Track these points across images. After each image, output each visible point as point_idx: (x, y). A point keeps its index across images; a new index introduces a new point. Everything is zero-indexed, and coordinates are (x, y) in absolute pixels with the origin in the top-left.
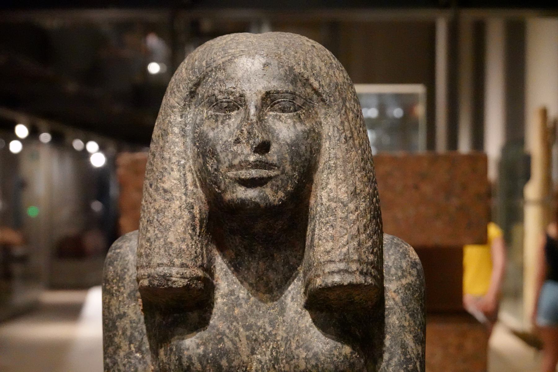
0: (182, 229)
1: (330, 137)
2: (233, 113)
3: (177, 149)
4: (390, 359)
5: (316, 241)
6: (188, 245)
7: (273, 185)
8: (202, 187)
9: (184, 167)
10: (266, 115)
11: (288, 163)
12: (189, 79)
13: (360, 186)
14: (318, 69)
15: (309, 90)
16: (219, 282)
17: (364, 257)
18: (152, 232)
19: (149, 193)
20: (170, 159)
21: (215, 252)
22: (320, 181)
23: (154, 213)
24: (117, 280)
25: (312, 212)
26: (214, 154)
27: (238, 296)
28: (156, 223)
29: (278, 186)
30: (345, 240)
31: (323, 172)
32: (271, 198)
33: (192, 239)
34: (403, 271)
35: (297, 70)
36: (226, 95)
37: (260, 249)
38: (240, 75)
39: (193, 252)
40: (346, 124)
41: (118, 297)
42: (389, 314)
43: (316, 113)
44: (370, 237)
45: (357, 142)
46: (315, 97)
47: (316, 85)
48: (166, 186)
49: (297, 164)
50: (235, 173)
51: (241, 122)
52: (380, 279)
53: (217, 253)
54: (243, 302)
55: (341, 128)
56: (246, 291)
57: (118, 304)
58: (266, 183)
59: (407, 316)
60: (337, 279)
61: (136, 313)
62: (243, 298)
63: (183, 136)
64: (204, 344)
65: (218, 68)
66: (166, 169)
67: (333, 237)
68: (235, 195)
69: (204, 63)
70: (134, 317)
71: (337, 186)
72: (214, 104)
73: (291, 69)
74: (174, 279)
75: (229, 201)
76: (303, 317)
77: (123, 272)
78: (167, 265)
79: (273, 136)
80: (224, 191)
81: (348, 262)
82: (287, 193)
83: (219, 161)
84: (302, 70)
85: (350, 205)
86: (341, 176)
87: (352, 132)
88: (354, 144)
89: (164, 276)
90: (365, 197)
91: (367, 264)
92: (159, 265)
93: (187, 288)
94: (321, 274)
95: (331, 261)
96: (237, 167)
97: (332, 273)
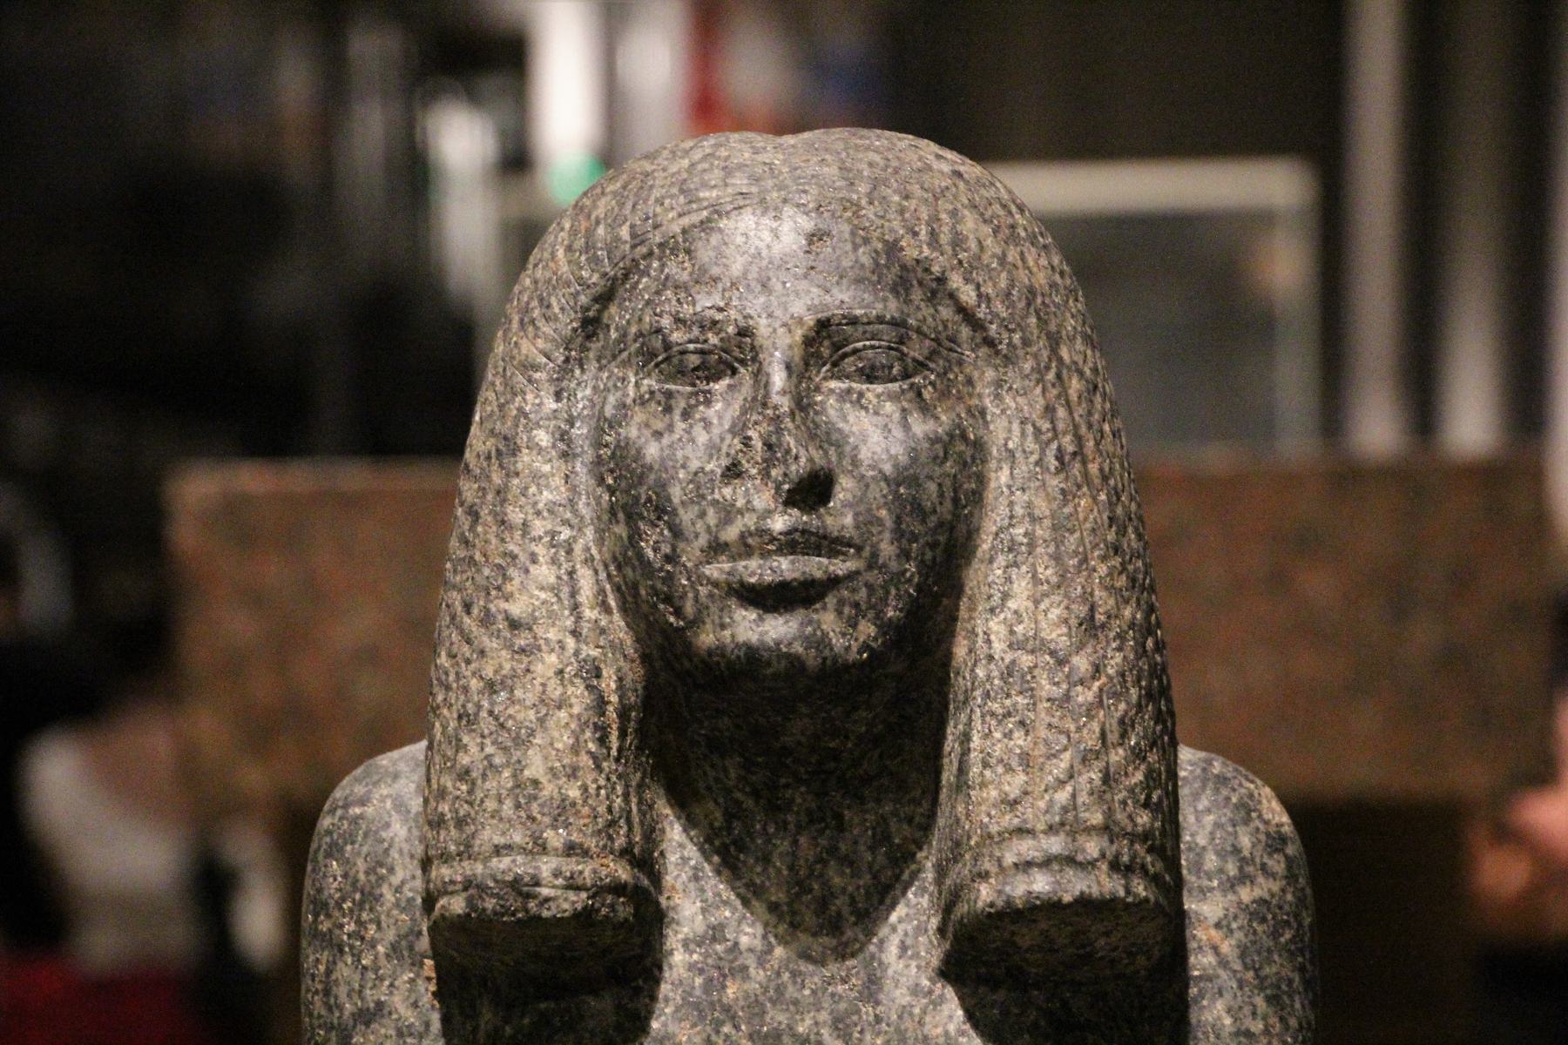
0: (566, 740)
1: (1011, 453)
2: (719, 386)
5: (975, 770)
6: (585, 788)
7: (841, 603)
8: (624, 610)
9: (569, 552)
10: (818, 389)
11: (887, 535)
12: (581, 281)
13: (1105, 602)
14: (973, 245)
15: (946, 312)
16: (677, 899)
17: (1120, 816)
18: (474, 749)
19: (462, 632)
21: (664, 809)
22: (985, 589)
23: (480, 692)
24: (354, 902)
25: (960, 684)
26: (662, 510)
27: (736, 944)
28: (487, 723)
29: (856, 605)
30: (1064, 765)
31: (991, 561)
32: (838, 642)
33: (599, 768)
34: (1243, 861)
35: (911, 252)
36: (696, 331)
37: (801, 798)
38: (736, 268)
39: (602, 809)
40: (1061, 413)
41: (357, 958)
42: (1202, 995)
43: (970, 382)
44: (1138, 755)
45: (1093, 468)
46: (965, 332)
47: (968, 295)
48: (516, 609)
49: (914, 538)
50: (727, 566)
51: (744, 411)
52: (1171, 885)
53: (668, 811)
54: (751, 961)
55: (1046, 426)
56: (759, 930)
57: (357, 977)
58: (821, 596)
59: (1259, 1001)
60: (1041, 884)
61: (415, 1005)
62: (751, 950)
63: (564, 455)
65: (669, 248)
66: (514, 557)
67: (1026, 759)
68: (727, 633)
69: (624, 232)
70: (410, 1017)
71: (1037, 603)
72: (660, 358)
73: (893, 248)
74: (545, 891)
75: (710, 652)
76: (938, 1003)
77: (373, 878)
78: (524, 850)
79: (841, 455)
80: (696, 623)
82: (884, 627)
83: (677, 533)
84: (926, 252)
85: (1076, 660)
86: (1048, 573)
87: (1079, 440)
88: (1086, 475)
89: (516, 884)
90: (1121, 637)
91: (1133, 837)
92: (498, 851)
93: (584, 917)
94: (994, 869)
95: (1022, 831)
97: (1026, 866)
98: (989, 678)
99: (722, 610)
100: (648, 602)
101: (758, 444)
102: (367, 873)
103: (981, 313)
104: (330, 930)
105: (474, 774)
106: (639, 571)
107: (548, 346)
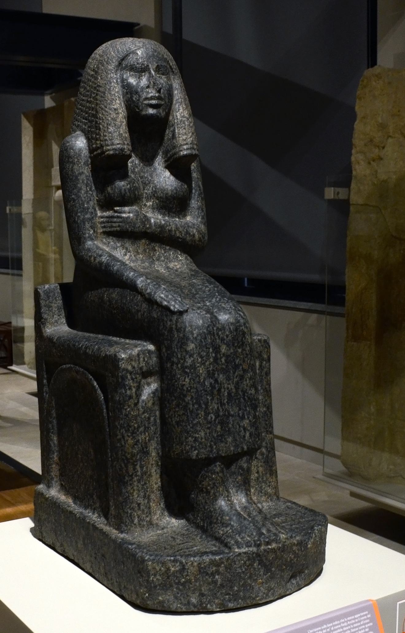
0: (124, 128)
3: (117, 90)
4: (195, 192)
12: (118, 57)
20: (114, 94)
41: (78, 165)
47: (171, 64)
48: (115, 107)
54: (138, 165)
64: (129, 184)
70: (87, 174)
74: (125, 150)
80: (142, 110)
81: (193, 145)
86: (184, 106)
98: (178, 122)
101: (152, 83)
103: (173, 67)
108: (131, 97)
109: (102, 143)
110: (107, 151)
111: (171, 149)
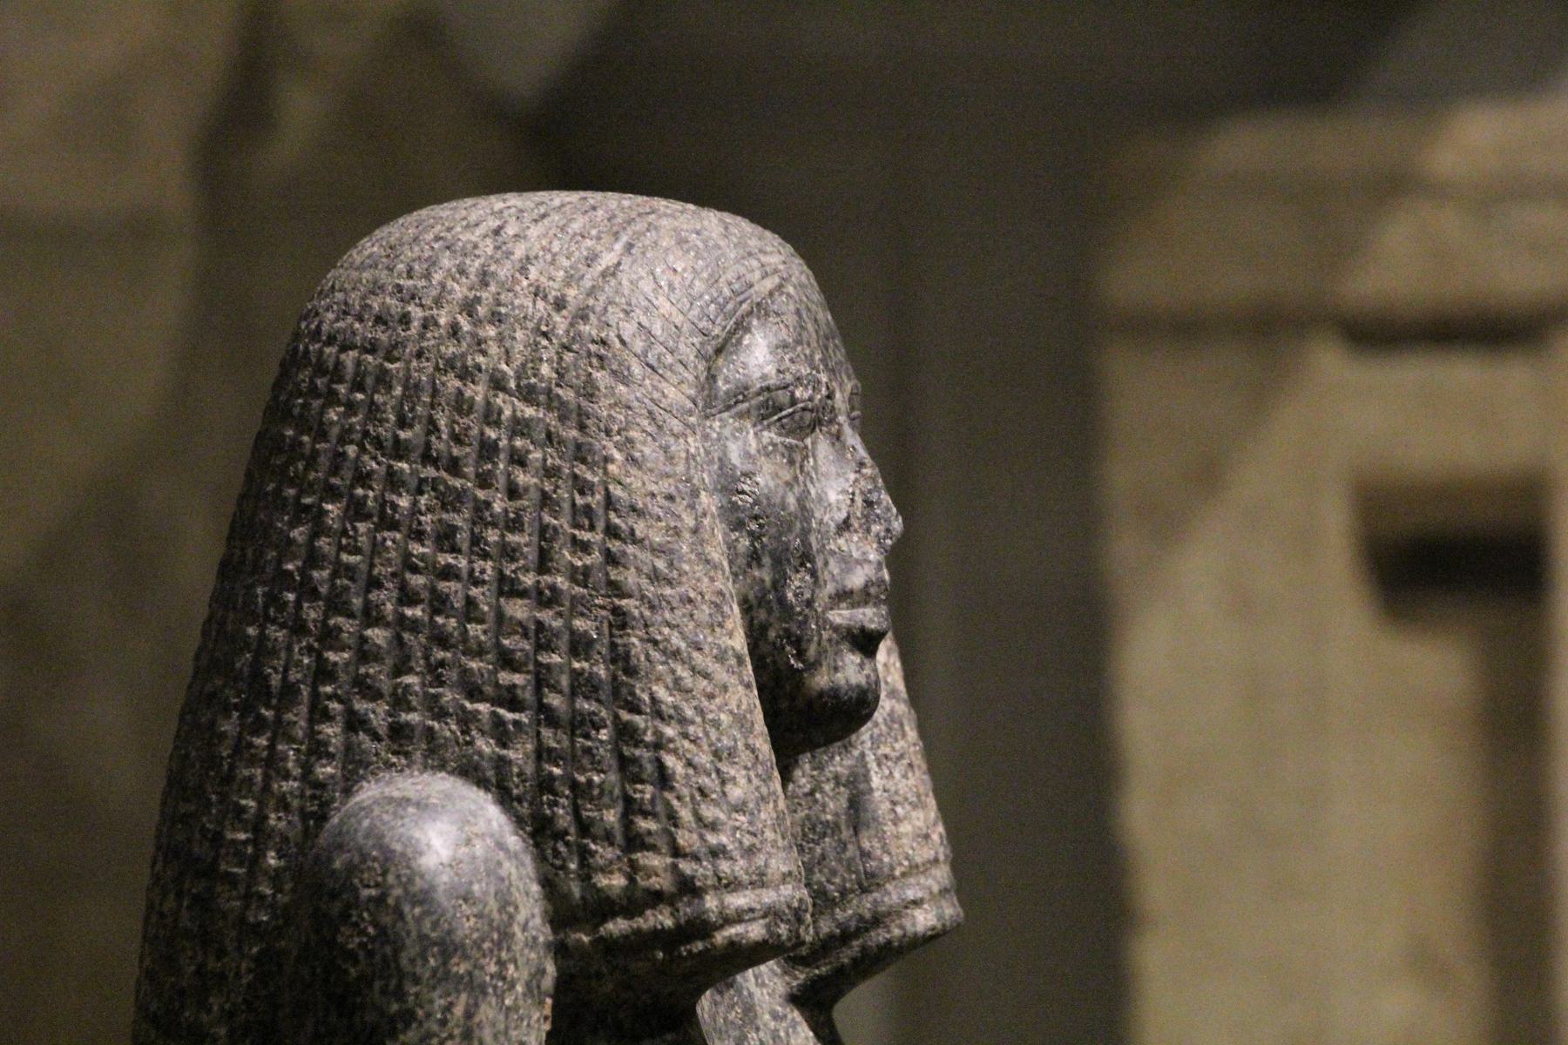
24: (492, 941)
41: (501, 998)
57: (502, 1017)
72: (784, 413)
75: (821, 694)
77: (505, 917)
80: (813, 666)
96: (856, 598)
99: (836, 654)
100: (774, 644)
102: (500, 911)
104: (470, 974)
105: (751, 805)
106: (777, 614)
107: (692, 392)
108: (775, 584)
109: (686, 867)
110: (728, 921)
111: (844, 893)
